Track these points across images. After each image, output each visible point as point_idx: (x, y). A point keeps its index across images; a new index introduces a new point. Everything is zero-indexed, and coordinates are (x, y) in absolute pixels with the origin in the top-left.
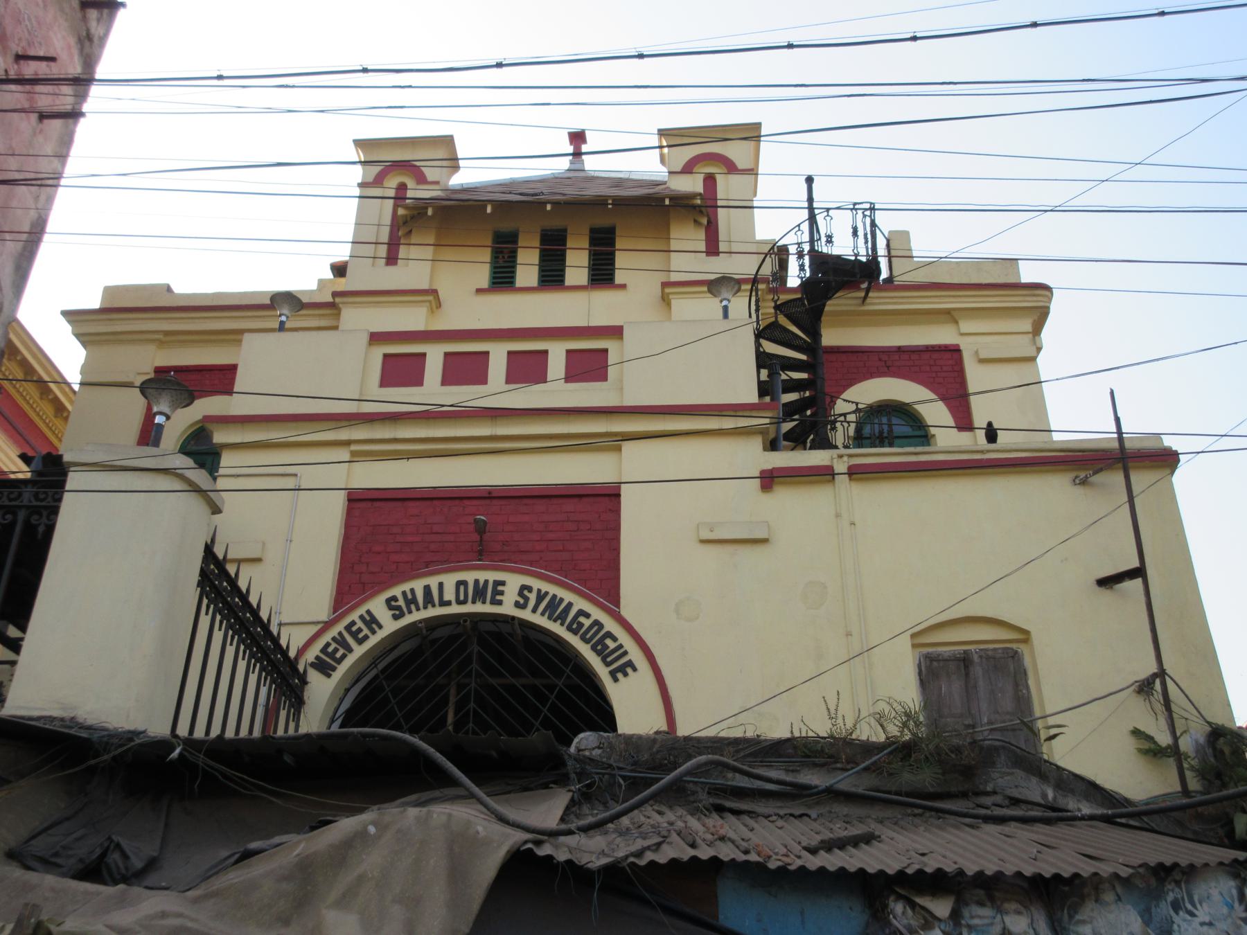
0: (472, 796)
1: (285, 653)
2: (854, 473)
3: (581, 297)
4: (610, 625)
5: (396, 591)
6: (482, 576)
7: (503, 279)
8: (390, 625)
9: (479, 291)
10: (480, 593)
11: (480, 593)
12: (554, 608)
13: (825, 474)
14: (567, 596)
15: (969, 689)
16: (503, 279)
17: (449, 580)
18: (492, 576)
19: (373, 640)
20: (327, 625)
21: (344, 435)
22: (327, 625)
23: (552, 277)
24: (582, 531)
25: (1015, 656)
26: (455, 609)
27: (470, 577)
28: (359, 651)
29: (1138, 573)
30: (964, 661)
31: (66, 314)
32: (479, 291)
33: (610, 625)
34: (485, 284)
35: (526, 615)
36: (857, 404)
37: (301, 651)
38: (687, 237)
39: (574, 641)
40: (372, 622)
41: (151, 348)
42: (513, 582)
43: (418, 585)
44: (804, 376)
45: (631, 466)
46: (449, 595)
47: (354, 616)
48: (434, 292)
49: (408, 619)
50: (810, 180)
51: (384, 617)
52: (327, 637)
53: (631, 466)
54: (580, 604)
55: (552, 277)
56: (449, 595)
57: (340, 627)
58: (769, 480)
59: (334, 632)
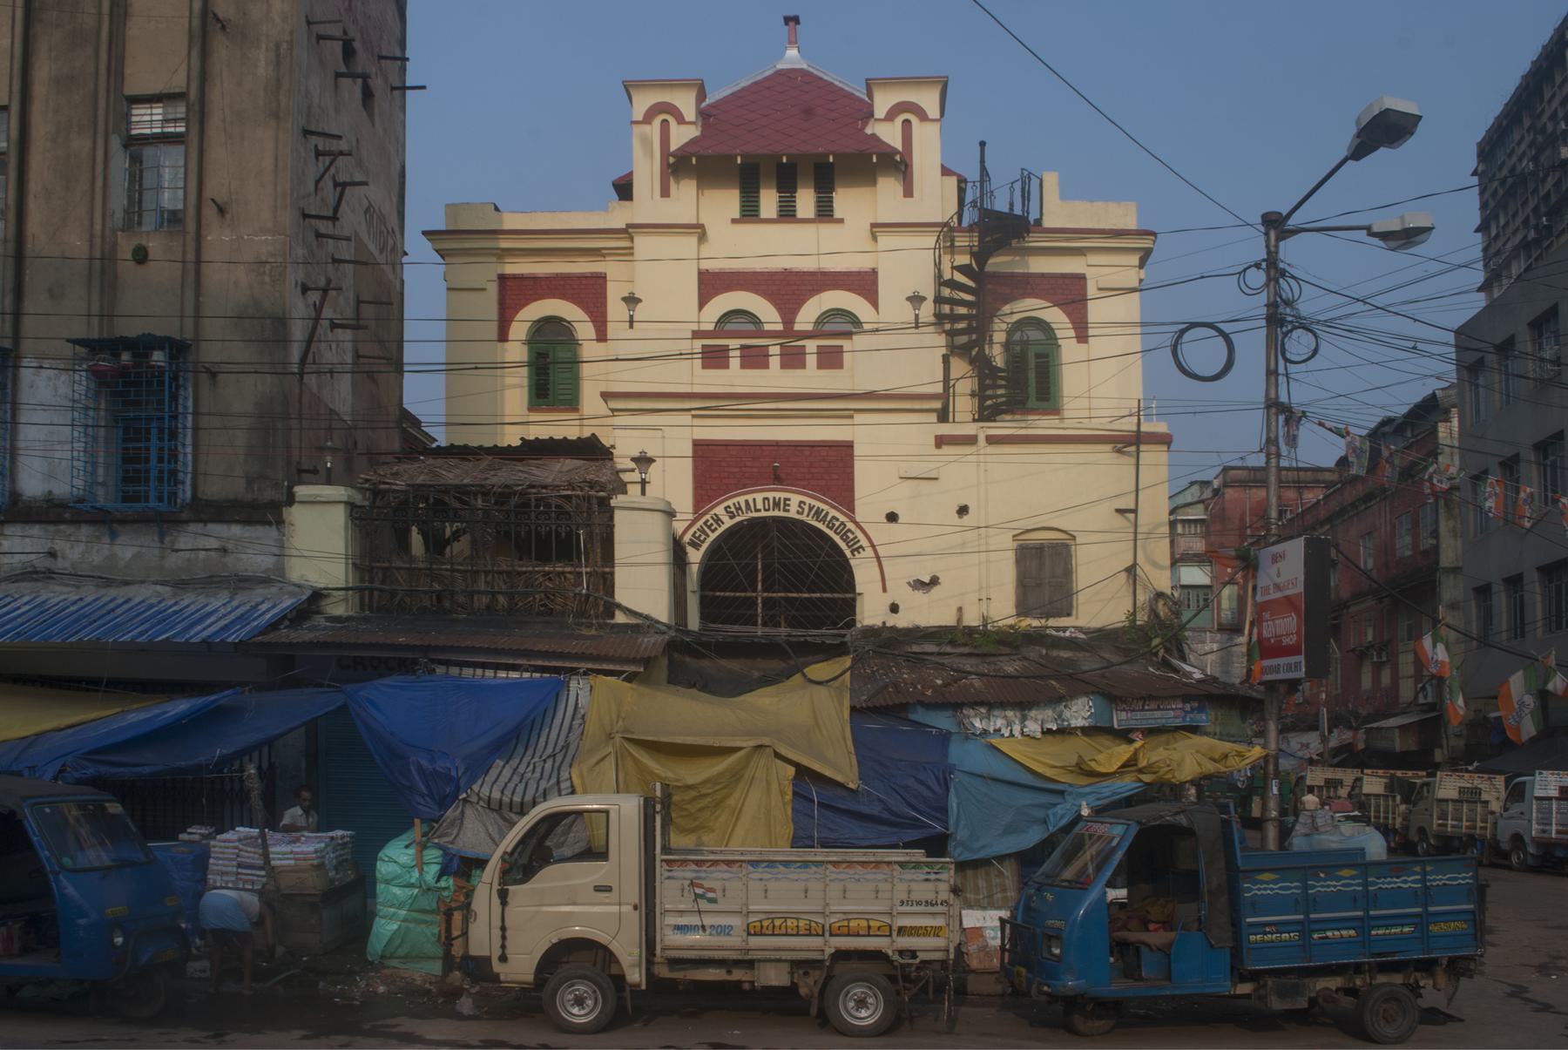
0: (841, 704)
4: (850, 525)
6: (778, 495)
7: (750, 212)
8: (728, 522)
9: (734, 221)
10: (777, 504)
11: (777, 504)
16: (750, 212)
17: (759, 497)
18: (783, 495)
19: (720, 530)
22: (694, 522)
23: (787, 213)
24: (830, 469)
25: (1067, 546)
26: (763, 514)
27: (770, 495)
28: (713, 536)
29: (1135, 511)
31: (425, 233)
32: (734, 221)
33: (850, 525)
34: (737, 216)
35: (803, 517)
38: (888, 186)
40: (718, 520)
42: (795, 499)
43: (741, 499)
46: (760, 505)
48: (701, 226)
49: (738, 519)
50: (982, 144)
51: (725, 515)
52: (694, 529)
54: (833, 513)
56: (760, 505)
57: (701, 522)
58: (940, 441)
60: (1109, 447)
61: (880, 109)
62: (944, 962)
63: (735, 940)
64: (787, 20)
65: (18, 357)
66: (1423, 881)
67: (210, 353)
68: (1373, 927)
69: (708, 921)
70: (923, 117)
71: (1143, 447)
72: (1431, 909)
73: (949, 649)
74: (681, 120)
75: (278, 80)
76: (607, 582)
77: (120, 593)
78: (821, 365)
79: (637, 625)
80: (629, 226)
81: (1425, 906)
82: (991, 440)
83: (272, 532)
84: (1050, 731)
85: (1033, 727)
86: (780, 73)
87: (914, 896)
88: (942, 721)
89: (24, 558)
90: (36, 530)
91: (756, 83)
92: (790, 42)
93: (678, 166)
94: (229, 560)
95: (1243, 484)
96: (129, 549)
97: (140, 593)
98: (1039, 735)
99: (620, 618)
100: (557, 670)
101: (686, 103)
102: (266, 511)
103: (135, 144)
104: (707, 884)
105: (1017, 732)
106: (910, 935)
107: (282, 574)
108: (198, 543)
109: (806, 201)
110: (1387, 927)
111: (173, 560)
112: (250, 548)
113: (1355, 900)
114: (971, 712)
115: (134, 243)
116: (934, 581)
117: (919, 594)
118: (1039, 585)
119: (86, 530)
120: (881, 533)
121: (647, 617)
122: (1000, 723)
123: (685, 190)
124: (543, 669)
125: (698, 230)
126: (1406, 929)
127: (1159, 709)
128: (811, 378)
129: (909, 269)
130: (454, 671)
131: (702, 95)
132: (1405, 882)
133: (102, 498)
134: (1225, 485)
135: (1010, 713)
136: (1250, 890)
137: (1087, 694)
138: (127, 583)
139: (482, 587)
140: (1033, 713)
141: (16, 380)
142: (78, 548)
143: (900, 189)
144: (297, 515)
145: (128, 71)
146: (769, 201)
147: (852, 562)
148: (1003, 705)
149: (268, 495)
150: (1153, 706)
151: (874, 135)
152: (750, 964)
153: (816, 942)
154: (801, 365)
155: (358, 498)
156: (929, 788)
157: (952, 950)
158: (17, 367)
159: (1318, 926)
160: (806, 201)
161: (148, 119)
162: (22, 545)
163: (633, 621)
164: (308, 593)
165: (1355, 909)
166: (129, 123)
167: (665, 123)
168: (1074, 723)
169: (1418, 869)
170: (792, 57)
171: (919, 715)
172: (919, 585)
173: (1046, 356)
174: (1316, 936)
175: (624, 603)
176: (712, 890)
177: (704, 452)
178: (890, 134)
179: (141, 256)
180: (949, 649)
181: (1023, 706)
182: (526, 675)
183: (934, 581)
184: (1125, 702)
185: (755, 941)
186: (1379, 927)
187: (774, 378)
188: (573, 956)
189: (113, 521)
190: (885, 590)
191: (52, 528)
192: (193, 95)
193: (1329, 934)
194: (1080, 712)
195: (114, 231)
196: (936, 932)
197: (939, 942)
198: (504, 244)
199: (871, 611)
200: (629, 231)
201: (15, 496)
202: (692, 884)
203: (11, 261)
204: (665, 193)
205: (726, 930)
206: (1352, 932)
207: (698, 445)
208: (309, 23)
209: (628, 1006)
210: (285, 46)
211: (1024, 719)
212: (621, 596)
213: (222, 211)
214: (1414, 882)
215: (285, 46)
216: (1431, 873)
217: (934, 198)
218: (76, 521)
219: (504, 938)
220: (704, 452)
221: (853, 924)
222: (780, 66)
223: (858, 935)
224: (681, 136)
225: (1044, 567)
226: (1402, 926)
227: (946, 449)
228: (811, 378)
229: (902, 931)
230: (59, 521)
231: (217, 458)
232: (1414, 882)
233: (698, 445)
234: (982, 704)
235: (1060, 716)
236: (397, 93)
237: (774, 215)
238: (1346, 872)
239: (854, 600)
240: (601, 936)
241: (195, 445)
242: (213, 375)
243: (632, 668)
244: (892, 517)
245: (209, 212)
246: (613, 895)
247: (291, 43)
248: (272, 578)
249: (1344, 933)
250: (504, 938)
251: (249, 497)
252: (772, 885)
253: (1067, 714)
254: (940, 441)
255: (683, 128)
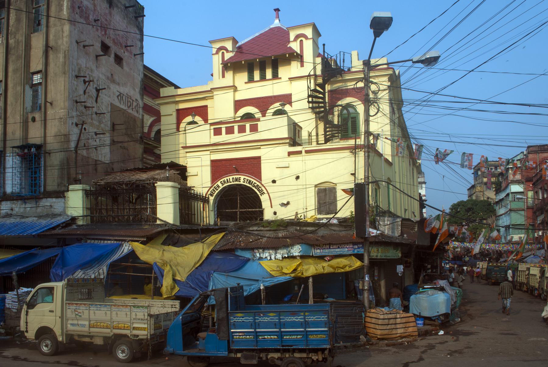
1: (203, 197)
2: (307, 152)
3: (271, 82)
5: (222, 180)
6: (237, 176)
7: (251, 79)
8: (221, 187)
9: (246, 83)
10: (236, 180)
11: (236, 180)
12: (250, 182)
13: (300, 152)
14: (252, 180)
15: (326, 195)
16: (251, 79)
17: (231, 177)
18: (238, 176)
19: (219, 190)
20: (211, 187)
21: (208, 149)
22: (211, 187)
23: (263, 78)
24: (253, 166)
27: (234, 177)
28: (217, 192)
30: (325, 190)
32: (246, 83)
35: (245, 184)
36: (412, 60)
37: (206, 195)
38: (295, 65)
39: (254, 188)
40: (218, 186)
41: (174, 105)
42: (242, 177)
43: (225, 179)
44: (323, 109)
45: (263, 153)
46: (231, 181)
47: (215, 185)
48: (234, 86)
52: (211, 190)
53: (263, 153)
54: (255, 181)
55: (263, 78)
56: (231, 181)
58: (290, 154)
59: (212, 188)
60: (348, 151)
61: (292, 38)
62: (147, 339)
63: (86, 329)
64: (275, 10)
65: (5, 154)
66: (304, 319)
67: (49, 147)
68: (285, 335)
69: (80, 322)
70: (306, 38)
71: (357, 150)
72: (282, 330)
73: (262, 229)
74: (227, 51)
75: (65, 62)
76: (154, 211)
77: (23, 220)
78: (240, 132)
79: (162, 224)
80: (211, 89)
81: (255, 329)
82: (307, 152)
83: (63, 200)
84: (285, 257)
85: (279, 256)
86: (271, 29)
87: (138, 317)
88: (247, 255)
89: (6, 211)
90: (9, 202)
91: (261, 34)
92: (276, 18)
93: (227, 66)
94: (52, 209)
95: (536, 152)
96: (29, 207)
97: (30, 219)
98: (281, 259)
99: (158, 222)
100: (119, 240)
101: (229, 45)
102: (60, 194)
103: (33, 86)
104: (79, 311)
105: (273, 257)
106: (137, 330)
107: (65, 213)
108: (46, 202)
109: (269, 73)
110: (290, 335)
111: (39, 210)
112: (56, 204)
113: (275, 324)
114: (257, 251)
115: (32, 116)
116: (288, 203)
117: (283, 208)
118: (325, 203)
119: (20, 202)
120: (271, 188)
121: (165, 221)
122: (267, 255)
123: (229, 75)
124: (116, 240)
125: (234, 88)
126: (299, 337)
127: (339, 248)
128: (248, 136)
129: (300, 91)
130: (93, 241)
131: (235, 41)
132: (297, 319)
133: (24, 193)
134: (528, 153)
135: (271, 251)
136: (233, 319)
137: (298, 244)
138: (27, 217)
139: (125, 214)
140: (279, 251)
141: (5, 160)
142: (18, 207)
143: (299, 64)
144: (70, 194)
145: (31, 65)
146: (257, 75)
147: (261, 197)
148: (268, 249)
149: (63, 189)
150: (335, 247)
151: (290, 47)
152: (91, 337)
153: (109, 330)
154: (233, 132)
155: (88, 188)
156: (204, 279)
157: (149, 335)
158: (5, 156)
159: (261, 334)
160: (269, 73)
161: (37, 79)
162: (6, 206)
163: (163, 223)
164: (70, 218)
165: (276, 328)
166: (33, 80)
167: (223, 53)
168: (295, 254)
169: (302, 314)
170: (276, 23)
171: (239, 253)
172: (283, 205)
173: (355, 118)
174: (260, 337)
175: (160, 218)
176: (80, 313)
177: (215, 164)
178: (295, 46)
179: (34, 120)
180: (262, 229)
181: (276, 248)
182: (112, 242)
183: (288, 203)
184: (319, 246)
185: (92, 330)
186: (287, 335)
187: (236, 137)
188: (44, 332)
189: (25, 199)
190: (272, 207)
191: (12, 202)
192: (43, 71)
193: (266, 337)
194: (296, 250)
195: (27, 113)
196: (144, 329)
197: (145, 333)
198: (177, 99)
199: (268, 215)
200: (212, 90)
201: (5, 193)
202: (75, 311)
203: (43, 122)
204: (223, 76)
205: (83, 326)
206: (275, 337)
207: (213, 162)
208: (77, 43)
209: (59, 350)
210: (67, 52)
211: (276, 253)
212: (159, 216)
213: (51, 104)
214: (301, 319)
215: (67, 52)
216: (308, 316)
217: (311, 64)
218: (17, 200)
219: (27, 325)
220: (215, 164)
221: (120, 325)
222: (272, 27)
223: (121, 329)
224: (228, 56)
225: (326, 196)
226: (297, 335)
227: (291, 156)
228: (248, 136)
229: (134, 328)
230: (13, 200)
231: (51, 179)
232: (301, 319)
233: (213, 162)
234: (260, 248)
235: (289, 252)
236: (138, 56)
237: (259, 79)
238: (271, 314)
239: (263, 211)
240: (51, 326)
241: (45, 175)
242: (50, 154)
243: (142, 239)
244: (274, 182)
245: (48, 104)
246: (54, 314)
247: (68, 50)
248: (64, 213)
249: (272, 337)
250: (27, 325)
251: (58, 190)
252: (118, 312)
253: (292, 251)
254: (290, 154)
255: (228, 54)
